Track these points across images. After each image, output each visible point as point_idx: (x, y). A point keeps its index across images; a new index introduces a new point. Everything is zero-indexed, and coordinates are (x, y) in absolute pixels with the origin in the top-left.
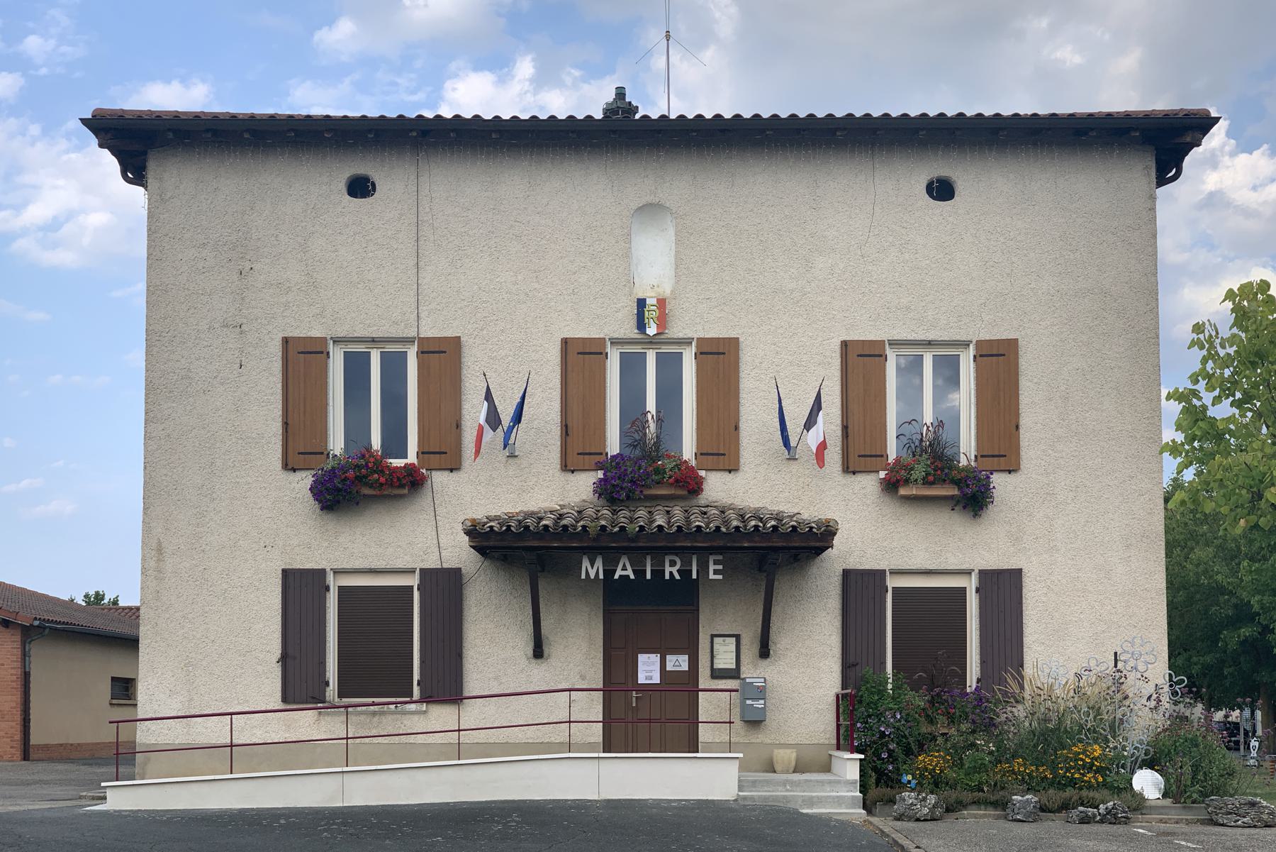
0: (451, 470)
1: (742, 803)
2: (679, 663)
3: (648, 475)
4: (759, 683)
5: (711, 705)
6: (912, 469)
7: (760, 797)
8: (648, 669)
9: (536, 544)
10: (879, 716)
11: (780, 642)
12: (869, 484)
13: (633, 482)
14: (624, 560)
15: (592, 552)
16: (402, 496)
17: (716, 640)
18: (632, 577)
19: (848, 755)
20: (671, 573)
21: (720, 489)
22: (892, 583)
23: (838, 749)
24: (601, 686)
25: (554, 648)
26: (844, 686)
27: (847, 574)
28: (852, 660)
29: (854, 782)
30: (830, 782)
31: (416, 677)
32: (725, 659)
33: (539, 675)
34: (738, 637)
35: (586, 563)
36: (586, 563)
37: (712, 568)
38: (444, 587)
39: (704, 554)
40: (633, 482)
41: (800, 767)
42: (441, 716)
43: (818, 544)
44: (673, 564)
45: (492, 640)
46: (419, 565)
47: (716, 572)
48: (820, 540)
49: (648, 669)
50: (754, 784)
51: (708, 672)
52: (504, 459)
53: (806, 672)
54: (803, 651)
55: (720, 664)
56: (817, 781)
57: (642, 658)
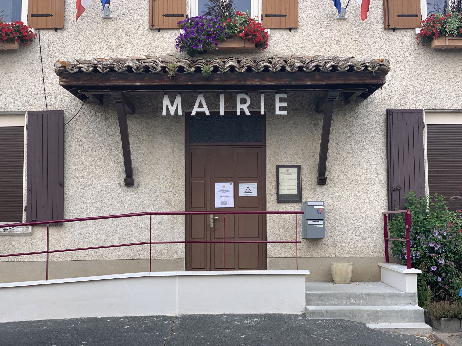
0: (56, 30)
1: (310, 317)
2: (249, 190)
3: (222, 29)
4: (318, 205)
5: (279, 226)
6: (446, 22)
7: (327, 311)
8: (224, 195)
9: (121, 83)
10: (427, 232)
11: (334, 171)
12: (406, 39)
13: (209, 35)
14: (200, 99)
15: (172, 90)
16: (13, 51)
17: (281, 170)
18: (208, 113)
19: (404, 270)
20: (242, 109)
21: (282, 46)
22: (428, 120)
23: (387, 261)
24: (183, 210)
25: (143, 177)
26: (390, 206)
27: (389, 113)
28: (396, 185)
29: (412, 296)
30: (391, 296)
31: (24, 204)
32: (289, 186)
33: (131, 200)
34: (299, 167)
35: (166, 101)
36: (166, 101)
37: (278, 105)
38: (49, 126)
39: (271, 91)
40: (209, 36)
41: (356, 278)
42: (38, 238)
43: (372, 82)
44: (243, 101)
45: (90, 169)
46: (27, 109)
47: (281, 108)
48: (373, 78)
49: (224, 195)
50: (321, 298)
51: (274, 197)
52: (101, 20)
53: (358, 194)
54: (354, 177)
55: (284, 191)
56: (378, 295)
57: (219, 186)
